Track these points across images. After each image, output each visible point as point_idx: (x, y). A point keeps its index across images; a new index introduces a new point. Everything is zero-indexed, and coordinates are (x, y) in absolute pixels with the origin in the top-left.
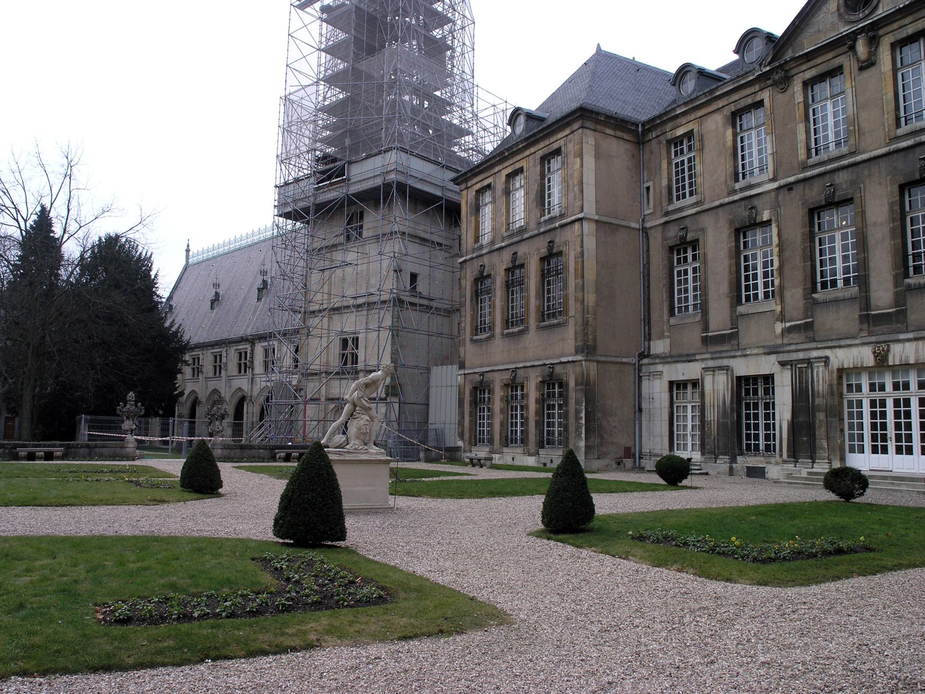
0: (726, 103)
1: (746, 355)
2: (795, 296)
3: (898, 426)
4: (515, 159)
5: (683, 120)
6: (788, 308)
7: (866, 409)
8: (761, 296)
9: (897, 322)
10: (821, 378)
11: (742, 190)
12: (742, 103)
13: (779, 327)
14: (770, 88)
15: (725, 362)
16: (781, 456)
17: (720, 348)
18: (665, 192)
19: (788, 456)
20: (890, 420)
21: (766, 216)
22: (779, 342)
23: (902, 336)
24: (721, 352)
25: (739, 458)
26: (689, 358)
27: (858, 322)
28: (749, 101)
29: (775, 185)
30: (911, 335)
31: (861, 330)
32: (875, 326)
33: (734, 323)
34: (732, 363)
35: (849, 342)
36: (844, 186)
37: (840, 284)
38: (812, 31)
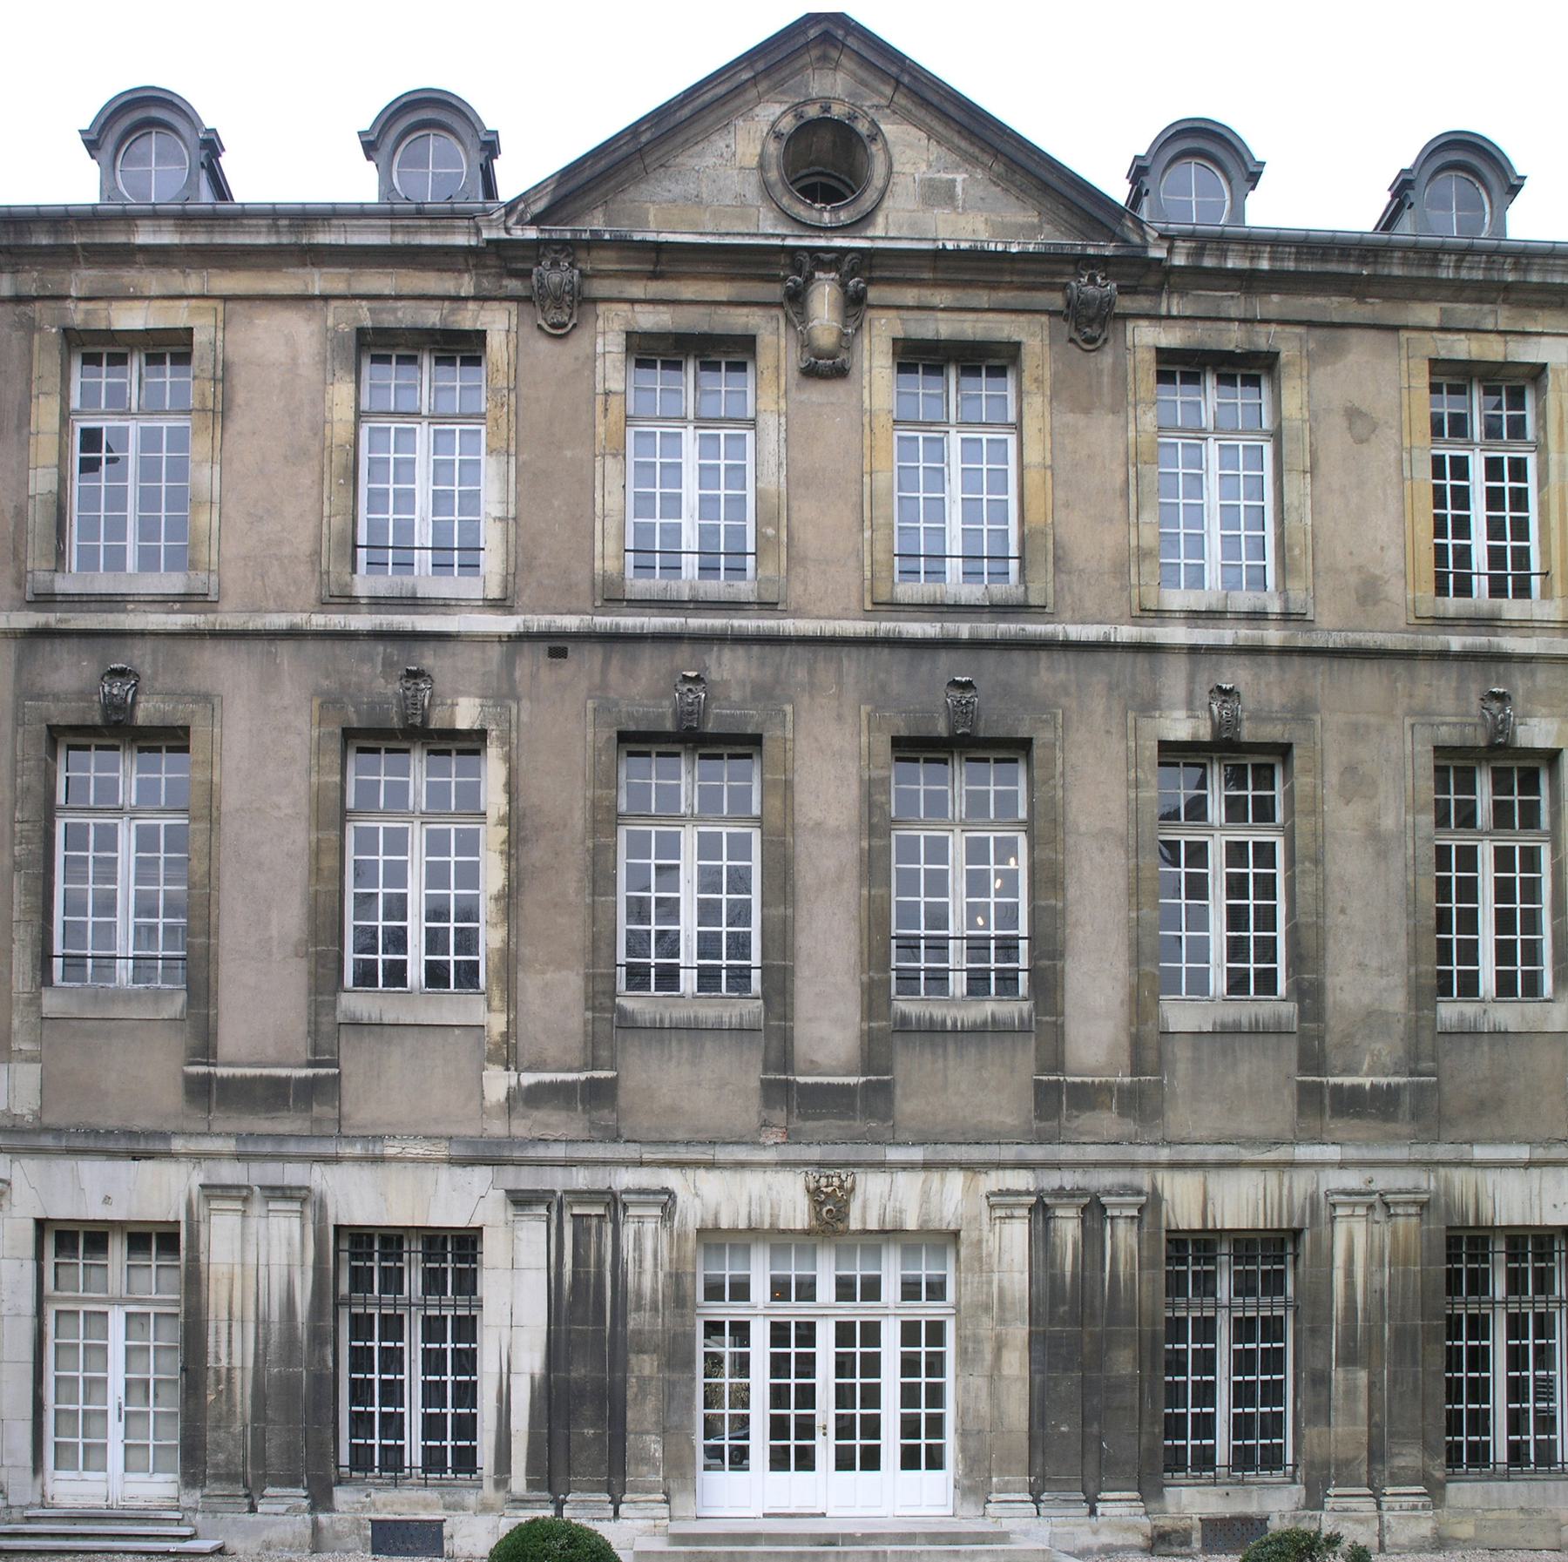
0: (339, 287)
1: (379, 1160)
2: (555, 998)
3: (843, 1396)
5: (153, 281)
6: (531, 1029)
7: (760, 1349)
8: (416, 973)
9: (872, 1116)
10: (645, 1251)
11: (378, 603)
12: (405, 316)
13: (498, 1083)
14: (513, 306)
15: (293, 1174)
16: (502, 1482)
17: (263, 1125)
18: (39, 517)
19: (531, 1485)
20: (825, 1379)
21: (466, 715)
22: (497, 1128)
23: (894, 1154)
24: (280, 1138)
25: (341, 1495)
26: (139, 1146)
27: (755, 1101)
28: (432, 316)
29: (509, 624)
30: (917, 1154)
31: (765, 1124)
32: (805, 1117)
33: (323, 1049)
34: (319, 1178)
35: (741, 1154)
36: (735, 695)
37: (688, 981)
38: (677, 189)
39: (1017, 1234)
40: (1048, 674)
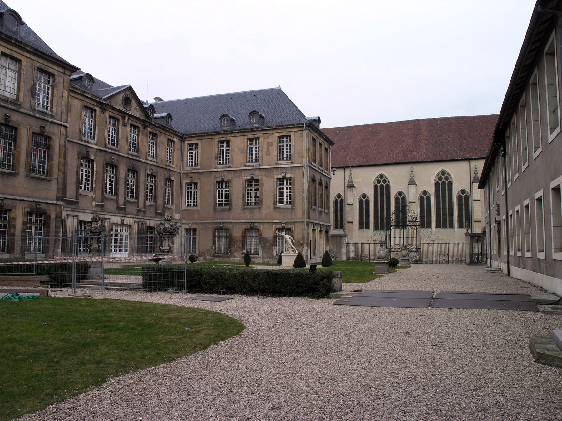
1: (84, 212)
4: (14, 49)
11: (85, 141)
12: (89, 105)
13: (94, 203)
15: (76, 213)
28: (92, 107)
29: (97, 147)
39: (137, 225)
40: (139, 164)
